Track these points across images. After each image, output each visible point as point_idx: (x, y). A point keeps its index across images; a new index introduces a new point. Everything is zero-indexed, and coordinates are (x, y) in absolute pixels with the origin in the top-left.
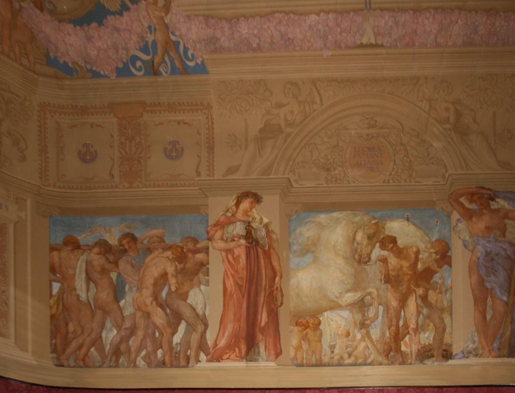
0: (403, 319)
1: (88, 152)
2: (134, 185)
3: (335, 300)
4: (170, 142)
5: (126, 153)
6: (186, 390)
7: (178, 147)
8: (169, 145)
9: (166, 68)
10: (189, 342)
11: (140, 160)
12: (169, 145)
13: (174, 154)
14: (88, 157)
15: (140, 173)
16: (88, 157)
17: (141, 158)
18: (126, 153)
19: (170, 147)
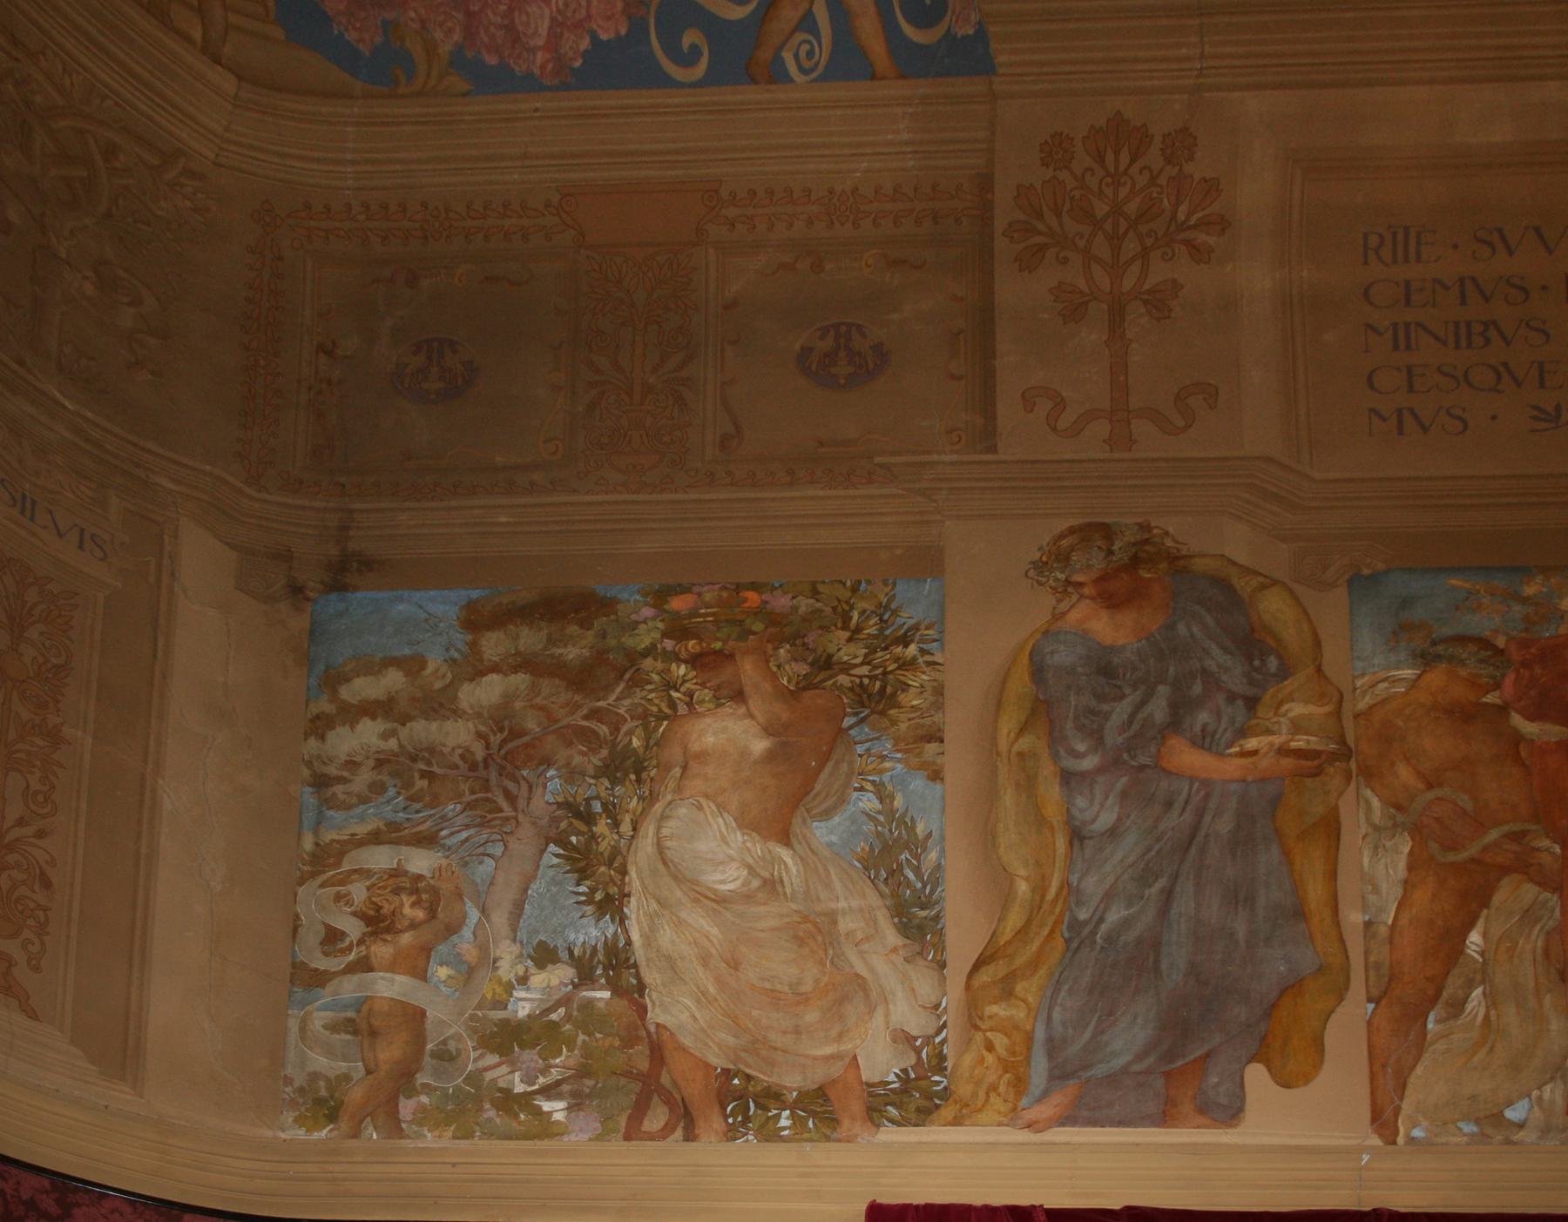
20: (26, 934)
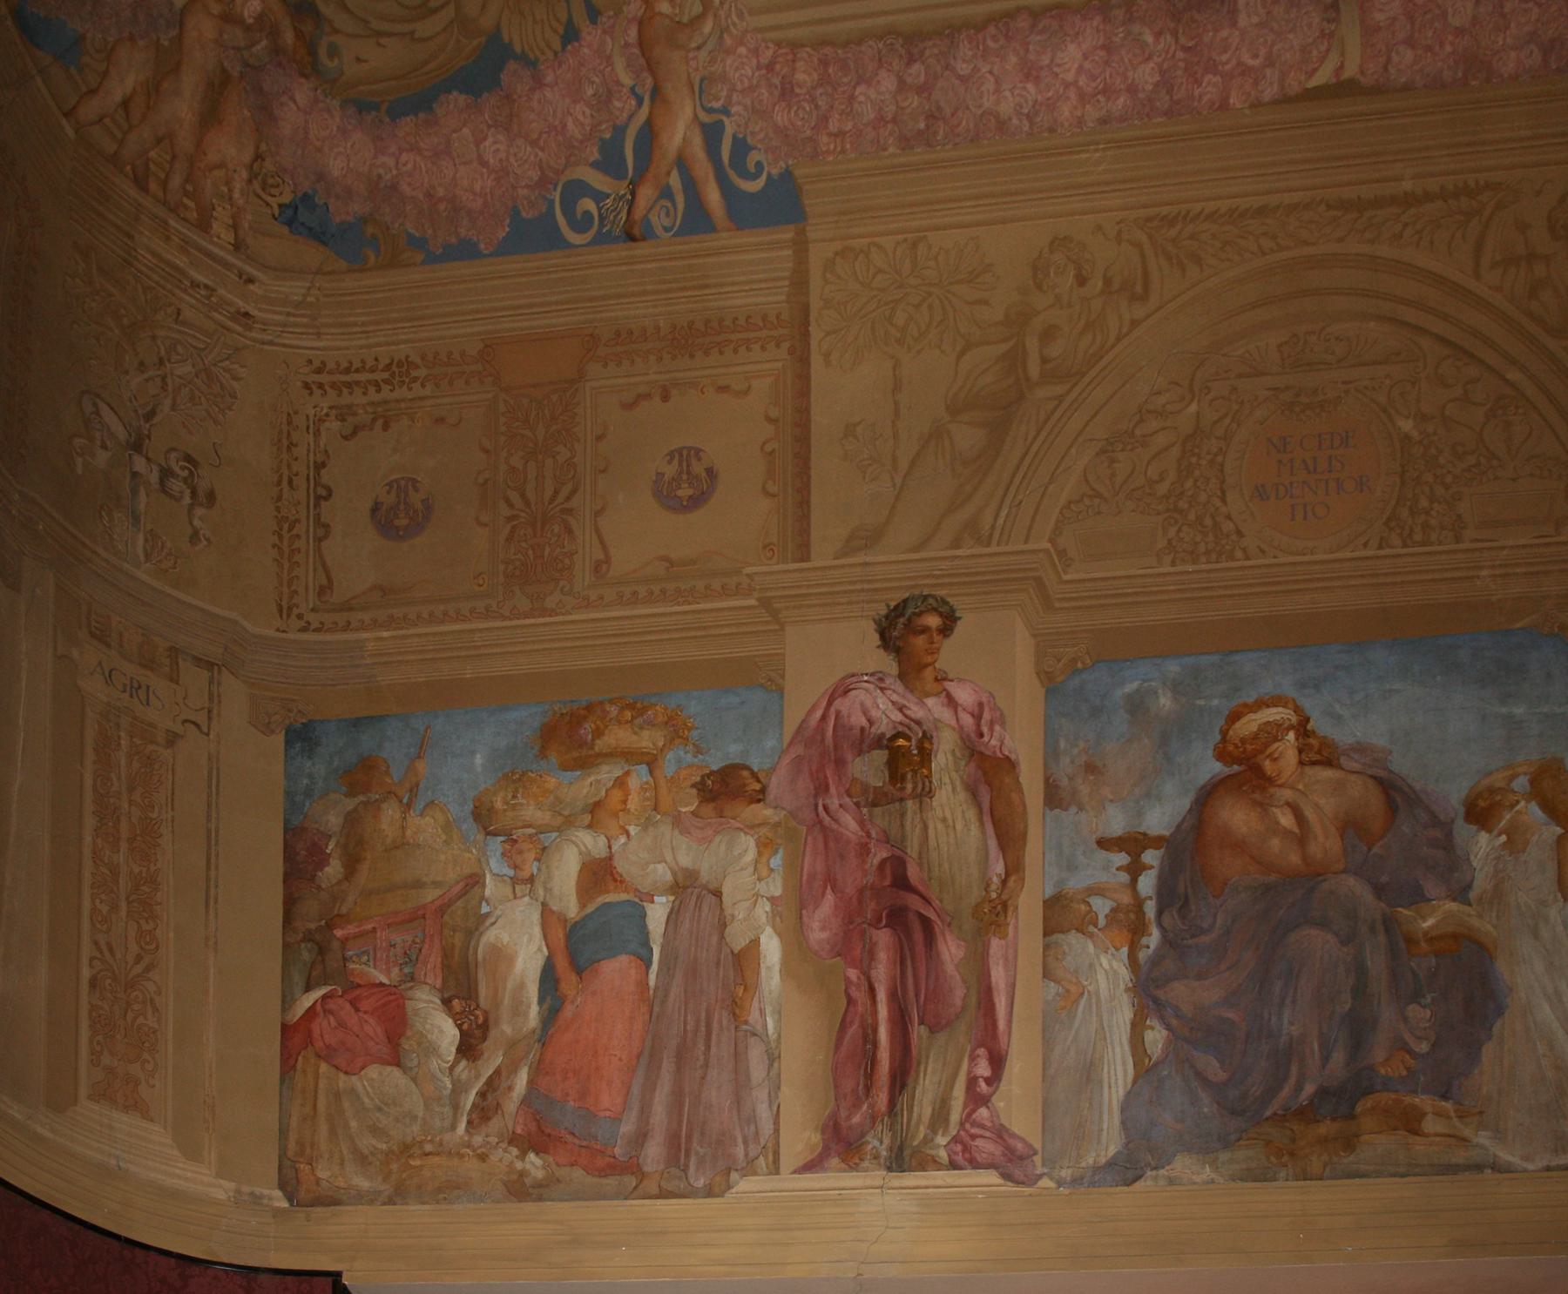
0: (774, 927)
1: (402, 507)
2: (550, 603)
3: (449, 911)
4: (390, 484)
5: (528, 504)
6: (77, 1227)
7: (698, 469)
8: (670, 462)
9: (668, 215)
10: (416, 1085)
11: (570, 519)
12: (670, 462)
13: (402, 522)
14: (685, 492)
15: (567, 561)
16: (402, 522)
17: (570, 511)
18: (528, 504)
19: (670, 471)
20: (146, 1056)
